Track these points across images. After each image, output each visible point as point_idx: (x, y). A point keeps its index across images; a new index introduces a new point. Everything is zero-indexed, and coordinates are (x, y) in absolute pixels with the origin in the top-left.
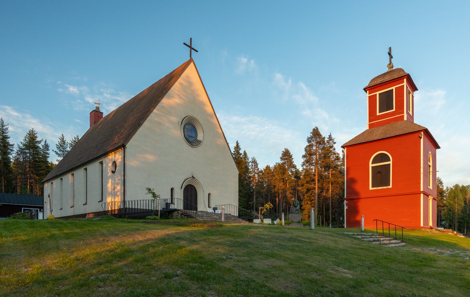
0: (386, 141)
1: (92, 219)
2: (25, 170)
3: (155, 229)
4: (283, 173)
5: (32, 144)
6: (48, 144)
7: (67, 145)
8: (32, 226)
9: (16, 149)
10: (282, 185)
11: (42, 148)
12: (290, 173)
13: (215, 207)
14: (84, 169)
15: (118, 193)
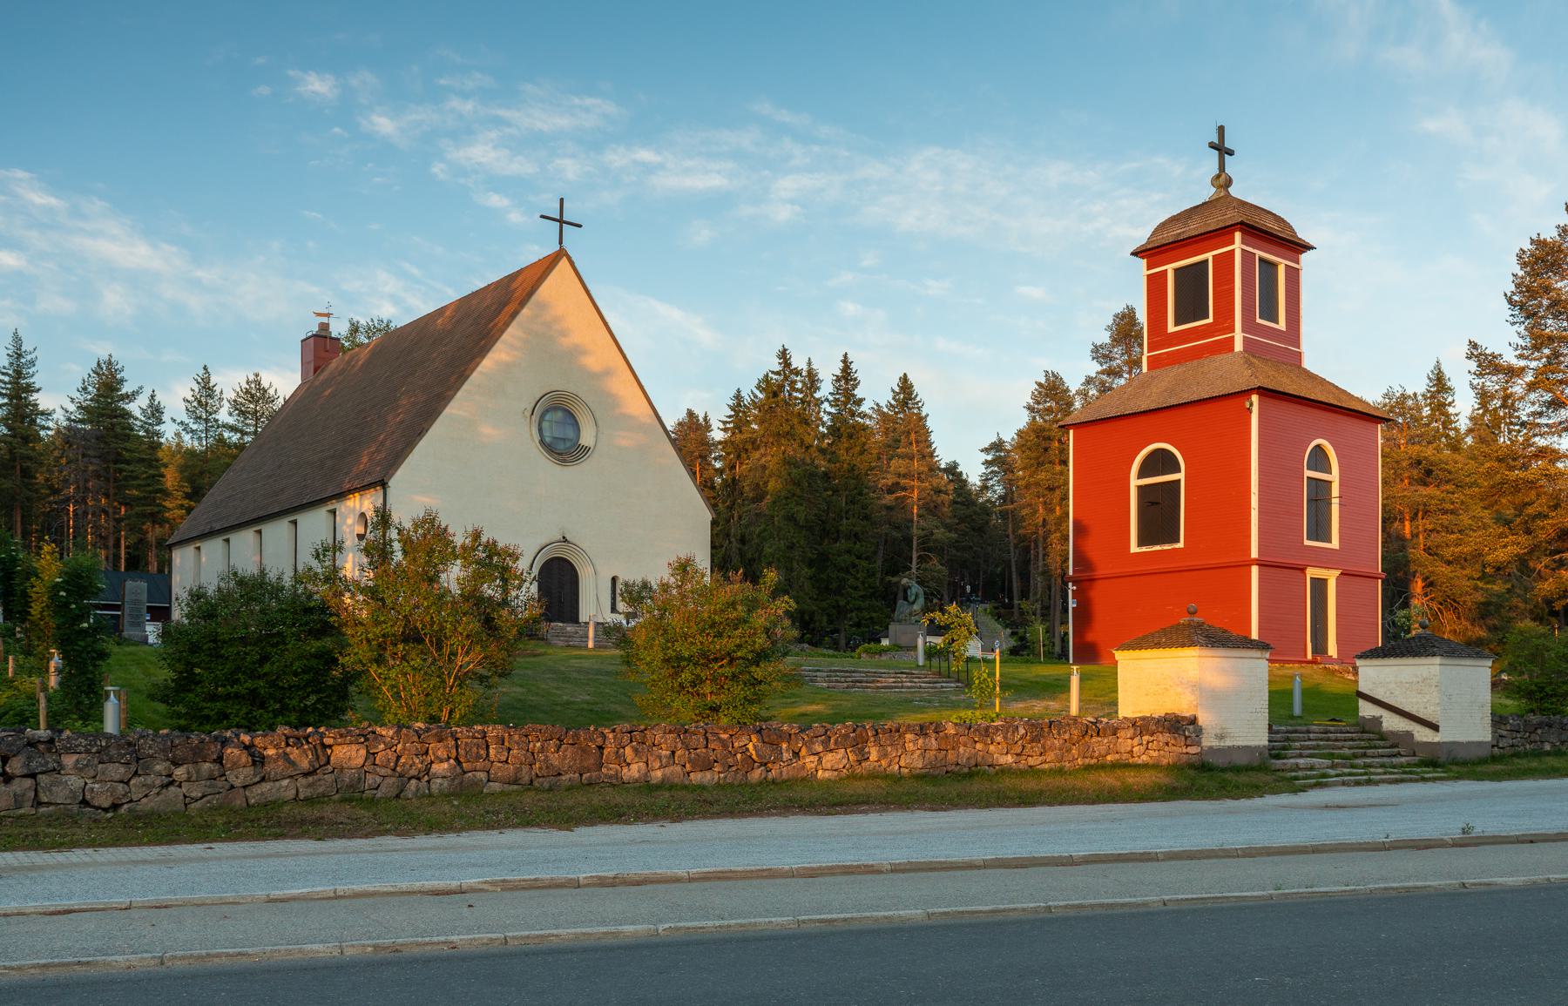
0: (1123, 423)
6: (159, 402)
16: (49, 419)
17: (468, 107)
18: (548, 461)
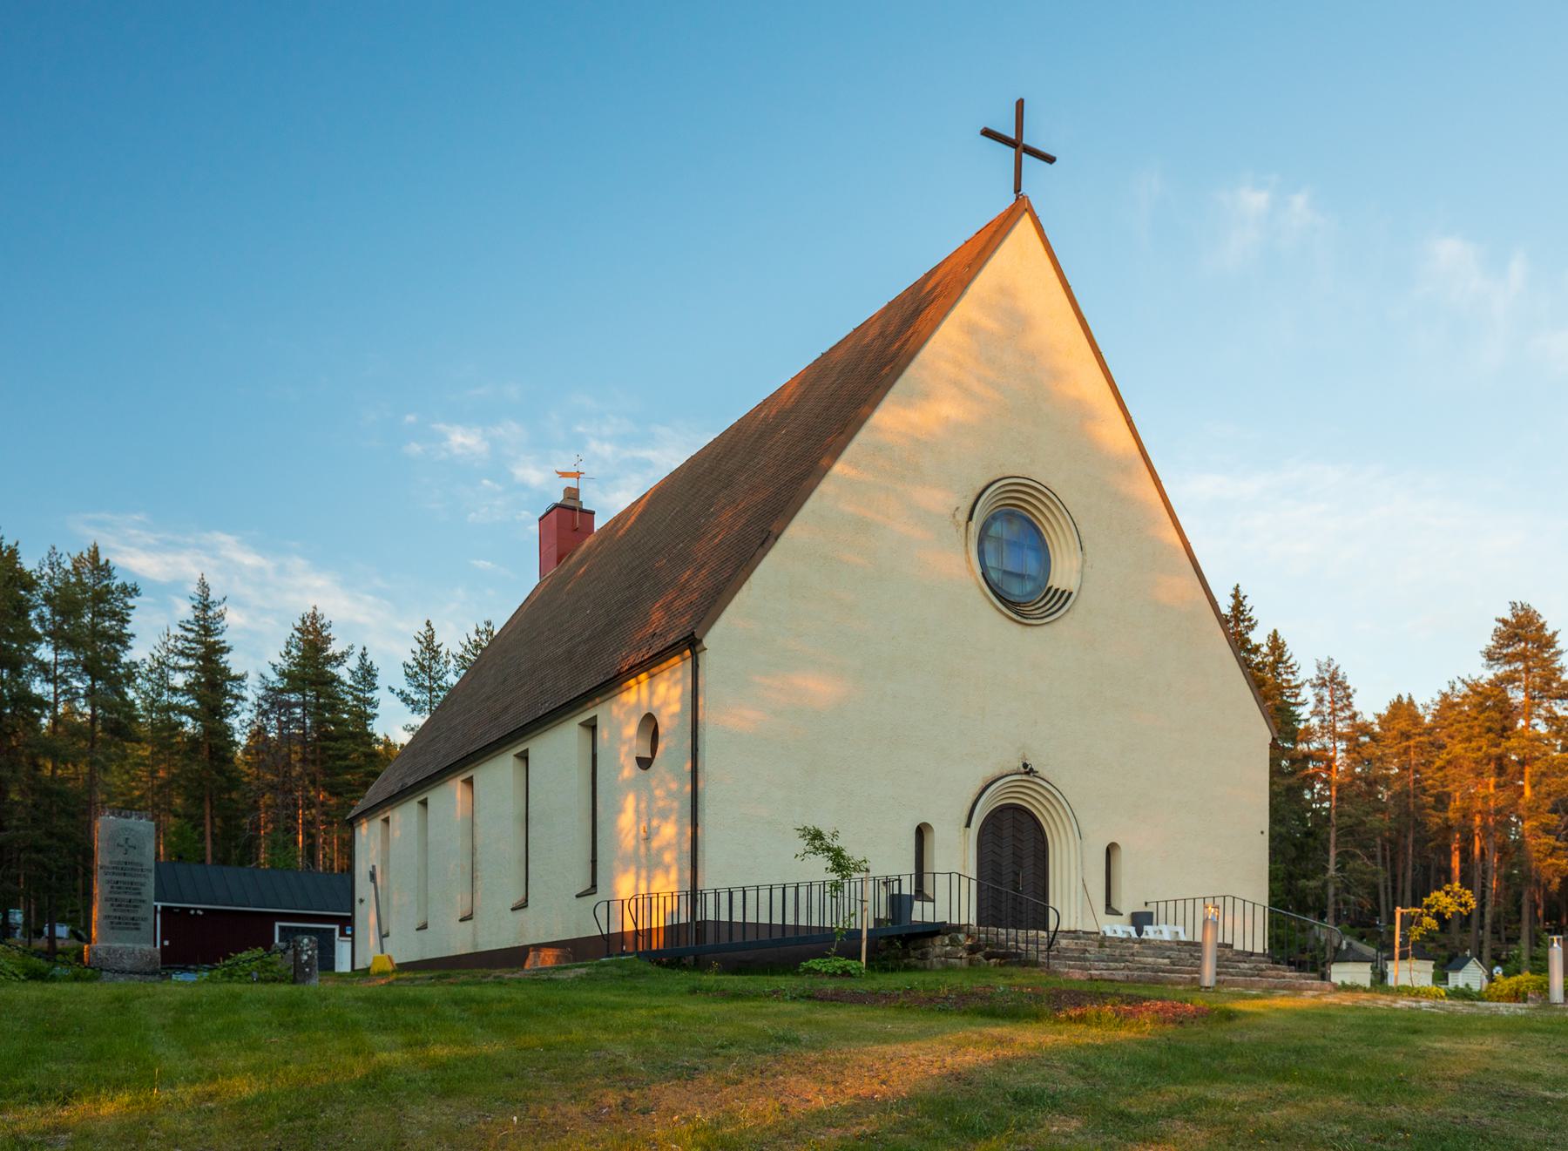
1: (553, 976)
2: (286, 772)
3: (886, 1039)
4: (1497, 727)
5: (314, 667)
6: (371, 663)
7: (447, 662)
8: (292, 1018)
9: (252, 692)
10: (1492, 790)
11: (352, 683)
12: (1542, 728)
13: (1142, 909)
14: (421, 802)
15: (668, 857)
16: (242, 687)
18: (997, 613)
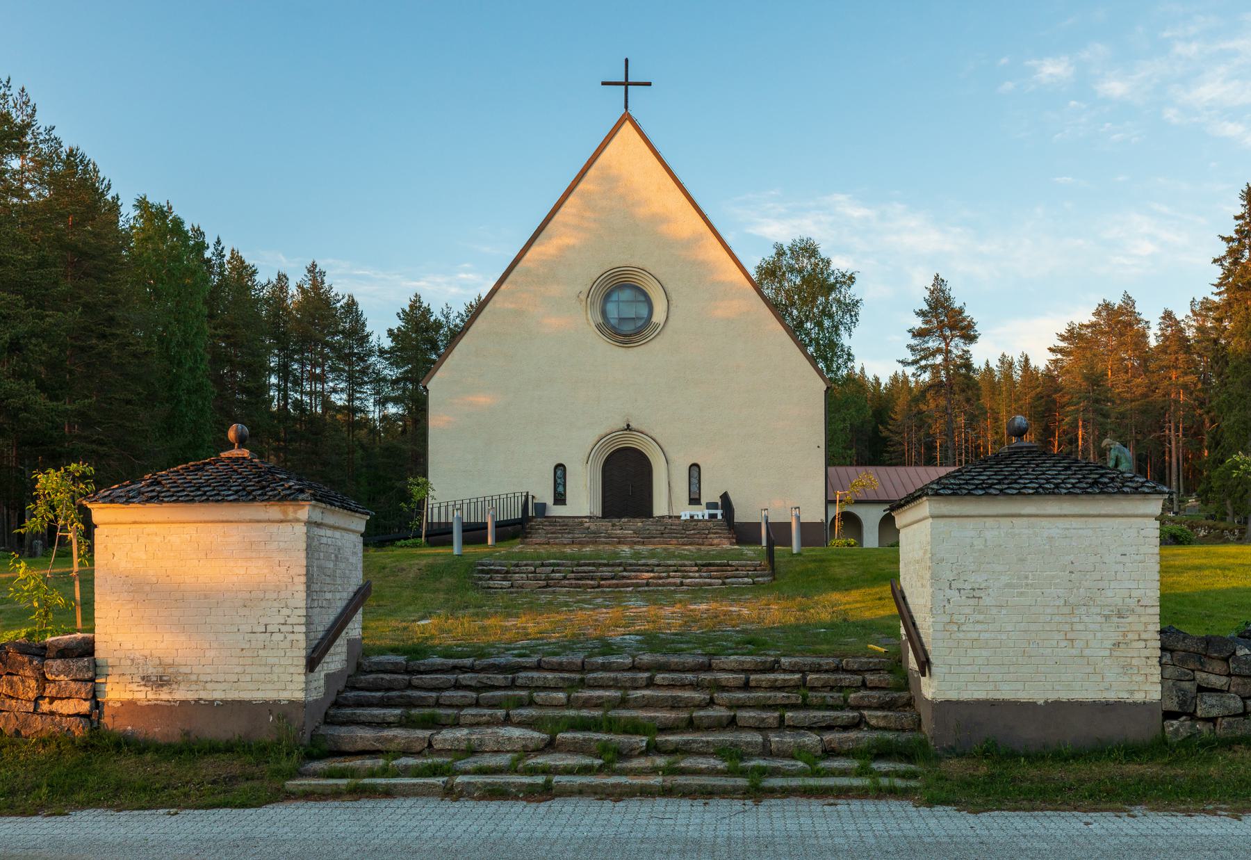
17: (1194, 48)
